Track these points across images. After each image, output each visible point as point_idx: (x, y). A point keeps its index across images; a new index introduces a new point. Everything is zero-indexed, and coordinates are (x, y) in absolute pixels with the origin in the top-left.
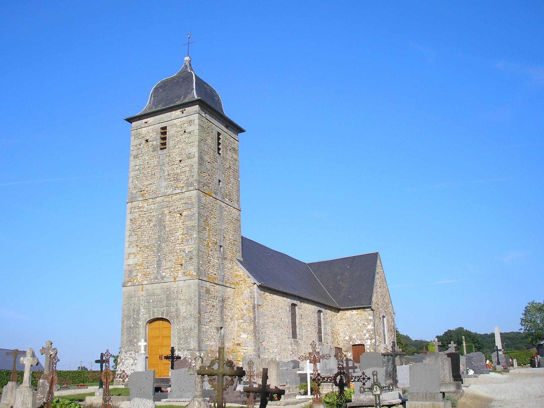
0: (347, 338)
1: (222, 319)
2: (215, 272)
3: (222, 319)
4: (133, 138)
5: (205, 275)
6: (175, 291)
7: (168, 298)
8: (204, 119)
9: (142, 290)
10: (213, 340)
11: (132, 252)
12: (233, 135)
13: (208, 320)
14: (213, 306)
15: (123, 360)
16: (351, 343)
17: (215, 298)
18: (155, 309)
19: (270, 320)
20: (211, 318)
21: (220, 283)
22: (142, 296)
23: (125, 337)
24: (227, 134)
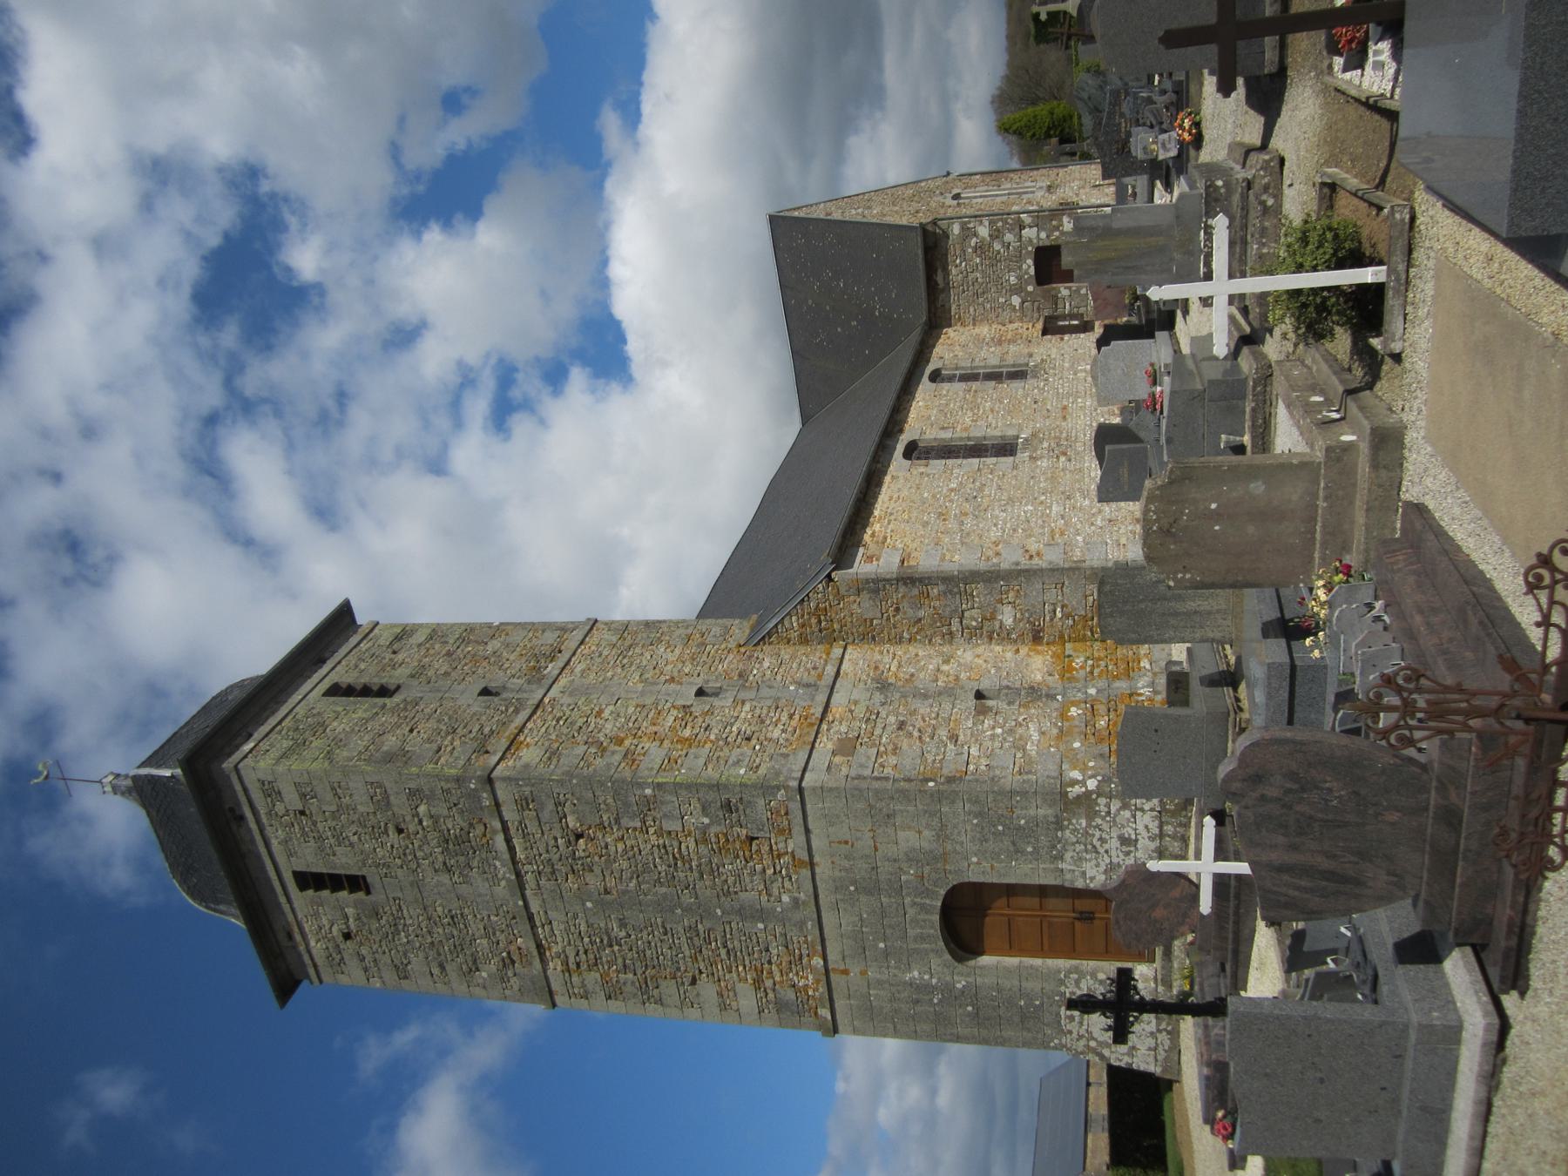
0: (1016, 301)
1: (949, 692)
2: (784, 718)
3: (949, 692)
4: (343, 979)
5: (786, 756)
6: (846, 864)
7: (872, 888)
8: (264, 746)
9: (845, 972)
10: (1020, 731)
11: (714, 999)
12: (354, 640)
13: (951, 746)
14: (901, 726)
15: (1093, 1044)
16: (1030, 288)
17: (872, 717)
18: (911, 932)
19: (952, 525)
20: (943, 733)
21: (821, 698)
22: (863, 973)
23: (1008, 1033)
24: (341, 667)
